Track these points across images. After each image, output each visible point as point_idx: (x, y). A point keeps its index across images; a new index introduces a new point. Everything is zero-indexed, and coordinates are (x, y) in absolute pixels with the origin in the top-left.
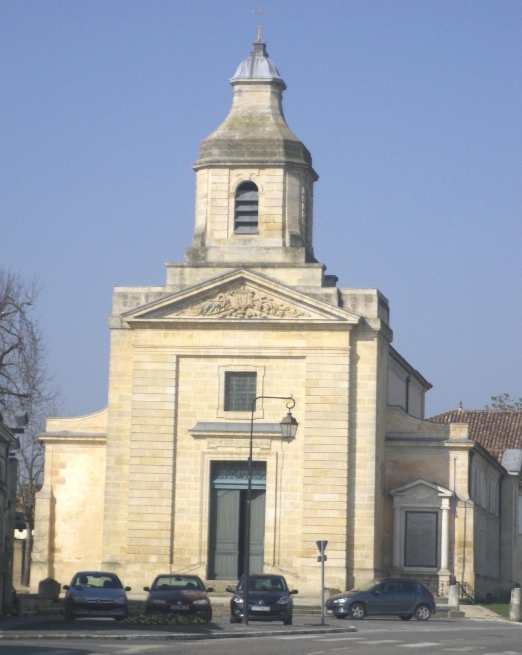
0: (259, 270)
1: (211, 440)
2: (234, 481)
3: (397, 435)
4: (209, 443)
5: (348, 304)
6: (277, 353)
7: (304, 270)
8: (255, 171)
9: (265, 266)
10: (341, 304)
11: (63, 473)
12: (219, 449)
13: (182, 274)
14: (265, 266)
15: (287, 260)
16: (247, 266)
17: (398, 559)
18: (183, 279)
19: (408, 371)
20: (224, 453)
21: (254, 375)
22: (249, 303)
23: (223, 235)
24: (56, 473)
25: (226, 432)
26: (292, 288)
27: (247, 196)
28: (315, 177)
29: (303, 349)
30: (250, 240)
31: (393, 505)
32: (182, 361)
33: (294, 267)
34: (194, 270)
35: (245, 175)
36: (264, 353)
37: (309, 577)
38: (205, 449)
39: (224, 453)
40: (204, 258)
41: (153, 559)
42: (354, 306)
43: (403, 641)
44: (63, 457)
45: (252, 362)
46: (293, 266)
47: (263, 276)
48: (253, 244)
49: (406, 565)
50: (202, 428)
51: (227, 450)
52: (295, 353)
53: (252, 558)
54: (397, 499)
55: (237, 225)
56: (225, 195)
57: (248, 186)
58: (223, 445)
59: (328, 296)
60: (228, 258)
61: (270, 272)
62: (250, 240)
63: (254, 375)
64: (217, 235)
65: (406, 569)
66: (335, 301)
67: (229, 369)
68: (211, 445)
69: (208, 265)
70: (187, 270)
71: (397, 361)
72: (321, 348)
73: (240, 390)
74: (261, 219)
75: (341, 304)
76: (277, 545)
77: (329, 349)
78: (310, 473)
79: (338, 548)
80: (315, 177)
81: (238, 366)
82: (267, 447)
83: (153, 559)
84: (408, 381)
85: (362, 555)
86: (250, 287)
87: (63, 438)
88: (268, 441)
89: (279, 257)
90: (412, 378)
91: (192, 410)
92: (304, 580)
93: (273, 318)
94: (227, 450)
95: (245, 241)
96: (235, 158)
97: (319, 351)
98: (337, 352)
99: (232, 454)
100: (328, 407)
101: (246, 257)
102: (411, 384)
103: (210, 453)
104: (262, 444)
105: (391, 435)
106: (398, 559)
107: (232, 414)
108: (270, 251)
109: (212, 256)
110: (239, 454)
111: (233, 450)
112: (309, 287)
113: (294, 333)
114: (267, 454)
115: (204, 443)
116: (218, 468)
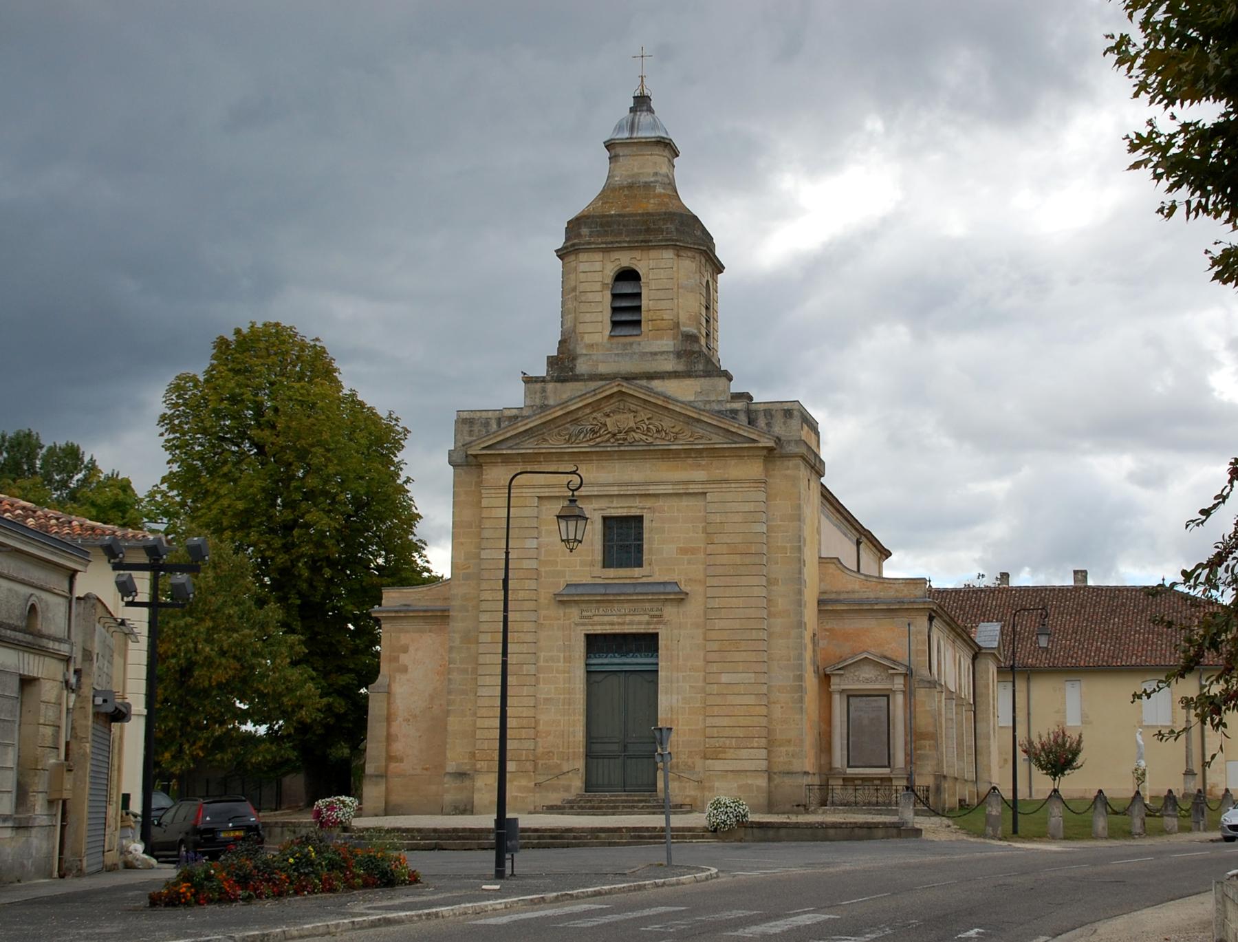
0: (644, 382)
1: (583, 606)
2: (606, 661)
3: (833, 596)
5: (762, 422)
6: (669, 489)
7: (703, 380)
8: (637, 254)
9: (651, 376)
10: (751, 422)
11: (404, 659)
13: (544, 391)
14: (651, 376)
15: (681, 367)
16: (629, 378)
17: (839, 760)
18: (546, 398)
19: (856, 530)
20: (602, 624)
21: (639, 519)
22: (632, 424)
23: (597, 338)
24: (396, 659)
25: (603, 596)
26: (689, 404)
27: (627, 288)
28: (719, 268)
29: (703, 482)
30: (631, 344)
31: (829, 686)
33: (690, 376)
34: (559, 385)
35: (625, 260)
36: (653, 490)
37: (717, 784)
38: (577, 620)
39: (602, 624)
40: (572, 369)
42: (768, 424)
43: (571, 924)
44: (404, 639)
45: (638, 502)
46: (688, 374)
47: (650, 390)
48: (636, 348)
49: (849, 766)
50: (573, 591)
51: (606, 619)
52: (693, 488)
54: (834, 680)
55: (615, 324)
56: (598, 287)
57: (628, 275)
58: (601, 612)
59: (734, 412)
60: (603, 369)
61: (657, 384)
62: (631, 344)
63: (639, 519)
64: (588, 339)
65: (849, 771)
66: (743, 418)
67: (608, 513)
68: (585, 614)
69: (576, 378)
70: (550, 386)
71: (831, 504)
72: (726, 481)
73: (624, 539)
74: (644, 316)
75: (751, 422)
77: (737, 481)
78: (715, 646)
79: (756, 745)
80: (719, 268)
81: (619, 509)
84: (858, 543)
85: (787, 754)
87: (403, 614)
89: (669, 365)
90: (863, 539)
91: (559, 568)
93: (661, 444)
94: (606, 619)
95: (625, 344)
96: (610, 239)
99: (612, 624)
100: (737, 559)
101: (627, 366)
102: (862, 546)
103: (583, 624)
104: (652, 610)
105: (825, 597)
106: (839, 760)
107: (612, 572)
108: (658, 357)
109: (582, 367)
110: (623, 624)
111: (615, 619)
112: (709, 402)
113: (690, 461)
114: (657, 623)
115: (574, 612)
116: (595, 643)
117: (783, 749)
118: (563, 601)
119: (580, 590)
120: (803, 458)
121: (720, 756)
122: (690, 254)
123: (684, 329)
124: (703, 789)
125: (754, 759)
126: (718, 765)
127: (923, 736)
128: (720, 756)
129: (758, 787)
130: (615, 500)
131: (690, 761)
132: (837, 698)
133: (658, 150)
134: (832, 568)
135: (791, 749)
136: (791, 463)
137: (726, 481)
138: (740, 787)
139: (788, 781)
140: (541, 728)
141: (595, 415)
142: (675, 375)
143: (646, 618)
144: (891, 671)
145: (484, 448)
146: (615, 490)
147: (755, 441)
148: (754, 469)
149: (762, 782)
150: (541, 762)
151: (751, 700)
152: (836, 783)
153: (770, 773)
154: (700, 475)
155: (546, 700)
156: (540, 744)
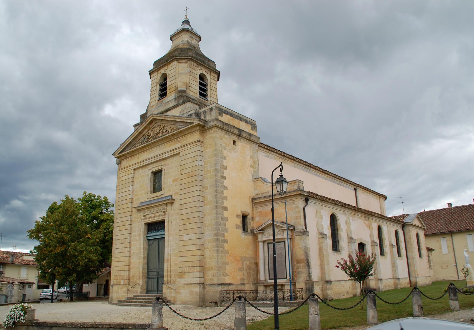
2: (155, 234)
4: (143, 213)
9: (167, 111)
12: (147, 216)
14: (167, 111)
32: (269, 245)
36: (165, 156)
38: (142, 217)
41: (122, 282)
53: (111, 288)
54: (259, 236)
61: (169, 113)
72: (186, 145)
76: (169, 271)
77: (190, 144)
78: (182, 222)
79: (195, 270)
82: (165, 210)
83: (122, 282)
84: (355, 189)
86: (159, 123)
88: (165, 206)
92: (179, 293)
97: (186, 147)
98: (193, 145)
103: (143, 219)
111: (152, 215)
114: (165, 215)
117: (210, 272)
118: (139, 210)
119: (145, 204)
120: (216, 126)
121: (183, 276)
122: (184, 61)
123: (179, 89)
124: (177, 293)
125: (194, 278)
126: (183, 281)
127: (299, 261)
128: (183, 276)
129: (196, 292)
130: (155, 164)
131: (175, 279)
132: (261, 245)
133: (183, 34)
134: (259, 183)
135: (213, 272)
136: (212, 131)
137: (186, 145)
138: (189, 292)
139: (212, 289)
140: (131, 266)
141: (149, 131)
142: (174, 107)
143: (162, 213)
144: (281, 229)
145: (119, 153)
146: (153, 160)
147: (193, 123)
148: (196, 136)
149: (197, 289)
150: (131, 280)
151: (193, 247)
152: (261, 288)
153: (203, 285)
154: (178, 145)
155: (133, 253)
156: (131, 273)
